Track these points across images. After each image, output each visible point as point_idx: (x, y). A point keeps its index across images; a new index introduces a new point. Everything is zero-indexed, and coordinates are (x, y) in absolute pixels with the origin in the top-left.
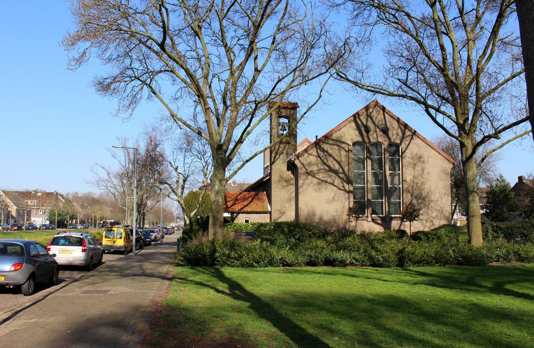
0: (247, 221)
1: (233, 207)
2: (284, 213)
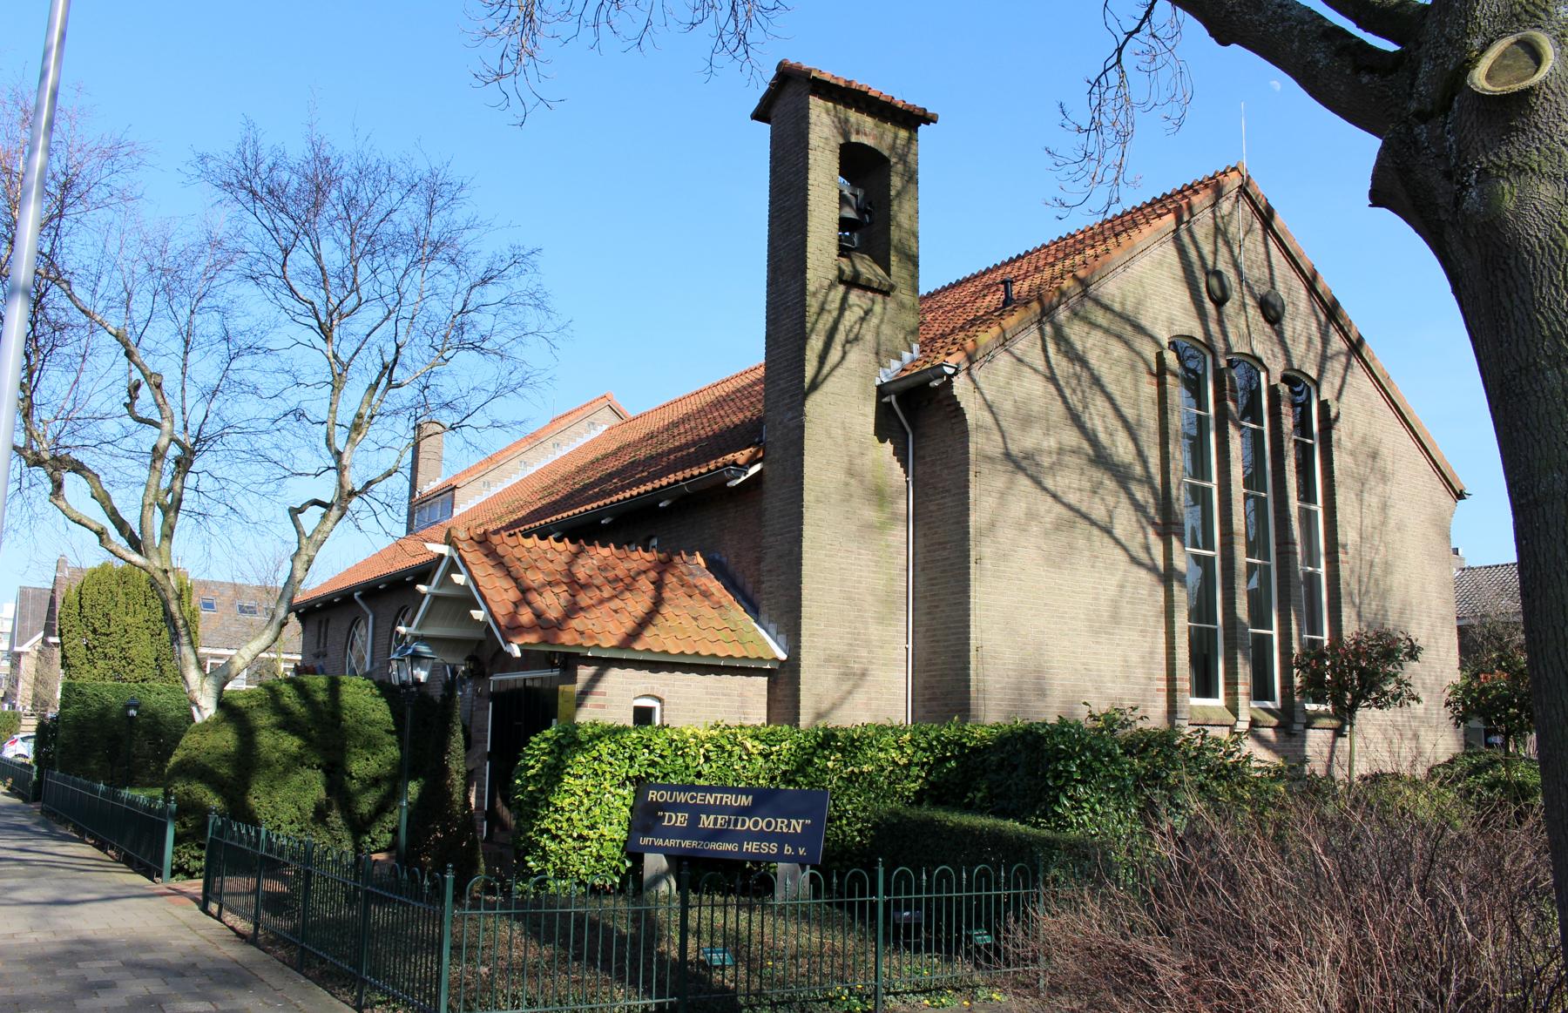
0: (643, 716)
1: (575, 623)
2: (863, 675)
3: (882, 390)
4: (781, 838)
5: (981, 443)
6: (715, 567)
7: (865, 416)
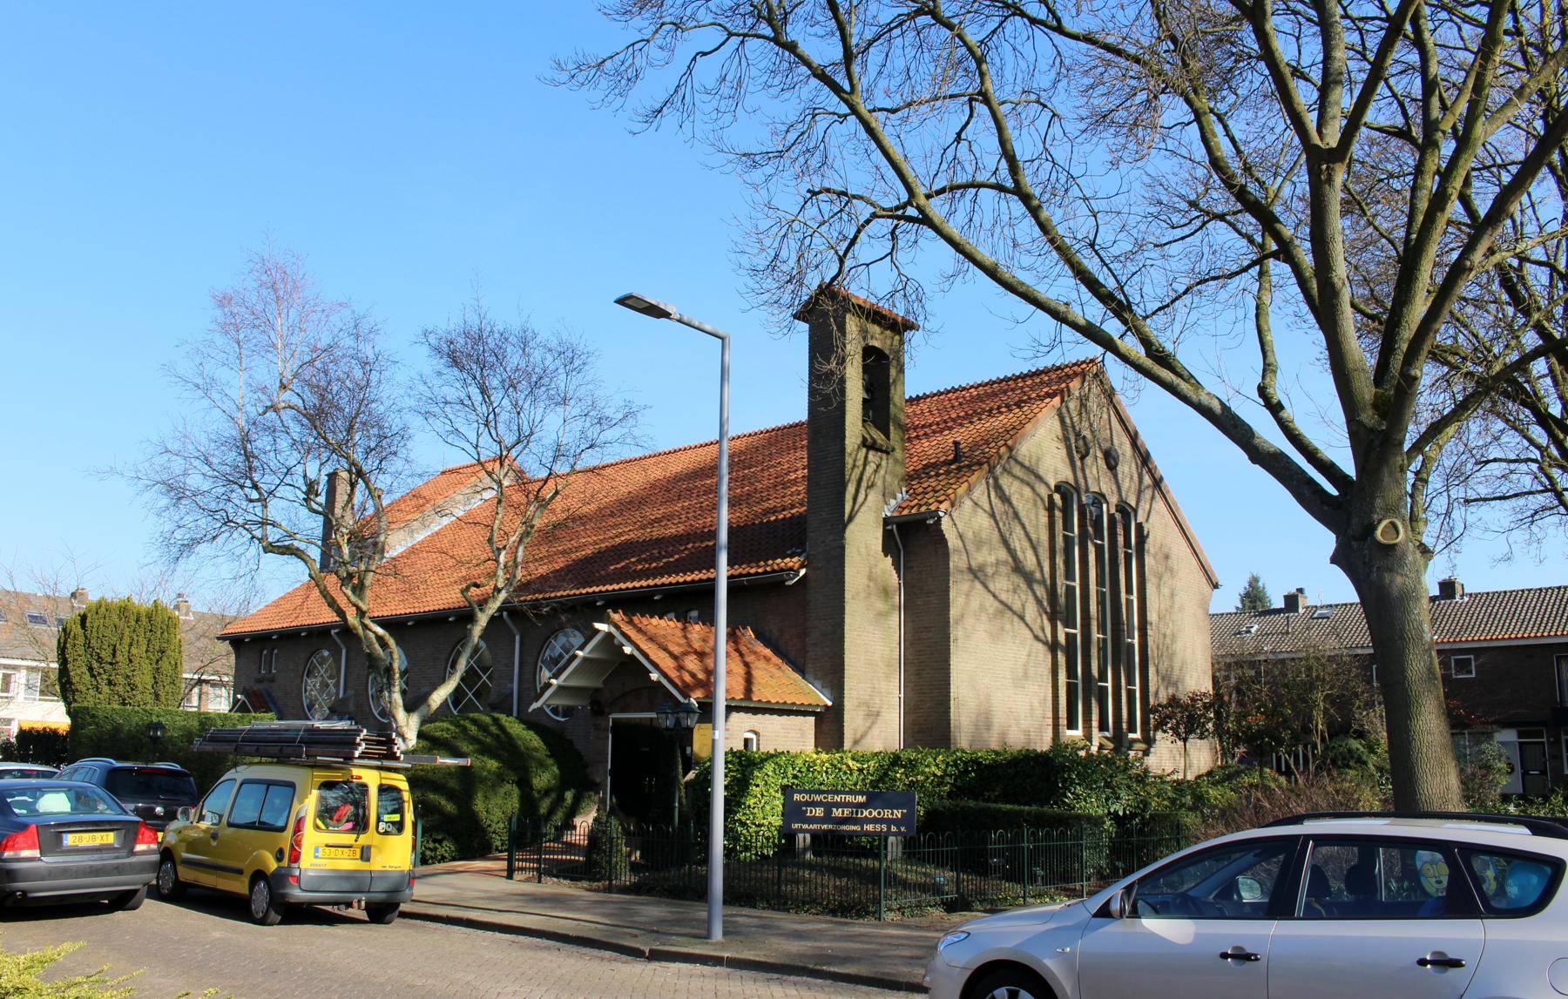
2: (878, 714)
3: (887, 521)
4: (889, 822)
5: (957, 561)
6: (760, 636)
7: (876, 538)
